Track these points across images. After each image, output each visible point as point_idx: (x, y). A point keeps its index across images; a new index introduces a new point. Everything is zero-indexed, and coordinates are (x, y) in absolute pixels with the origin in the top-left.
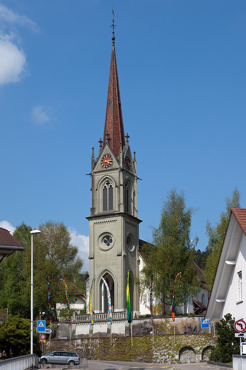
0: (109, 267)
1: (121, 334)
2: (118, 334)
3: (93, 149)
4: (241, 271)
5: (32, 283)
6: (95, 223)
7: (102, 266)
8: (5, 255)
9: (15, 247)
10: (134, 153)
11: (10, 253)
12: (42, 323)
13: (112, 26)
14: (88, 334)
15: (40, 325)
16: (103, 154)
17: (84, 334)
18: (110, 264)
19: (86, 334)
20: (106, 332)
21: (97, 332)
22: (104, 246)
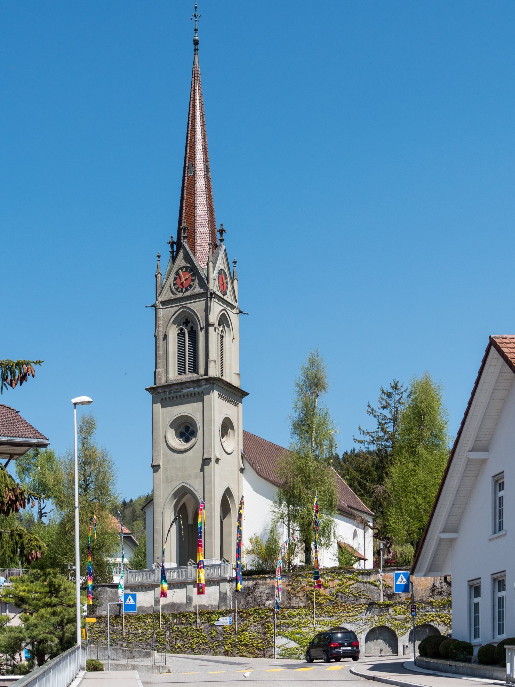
0: (189, 482)
1: (212, 606)
2: (207, 605)
3: (159, 256)
4: (503, 472)
5: (77, 504)
6: (162, 399)
7: (176, 480)
8: (11, 456)
9: (30, 439)
10: (234, 262)
11: (21, 452)
12: (131, 599)
13: (194, 18)
14: (152, 606)
15: (128, 601)
16: (177, 265)
17: (144, 607)
18: (190, 476)
19: (149, 605)
20: (184, 601)
21: (167, 603)
22: (176, 443)
